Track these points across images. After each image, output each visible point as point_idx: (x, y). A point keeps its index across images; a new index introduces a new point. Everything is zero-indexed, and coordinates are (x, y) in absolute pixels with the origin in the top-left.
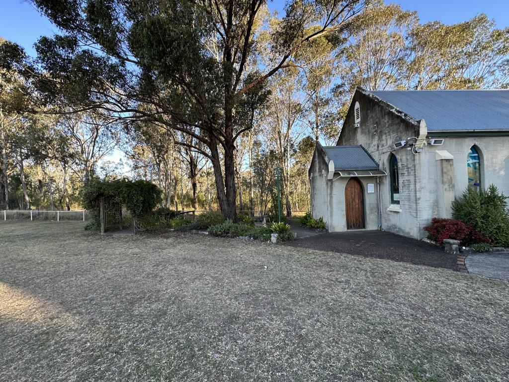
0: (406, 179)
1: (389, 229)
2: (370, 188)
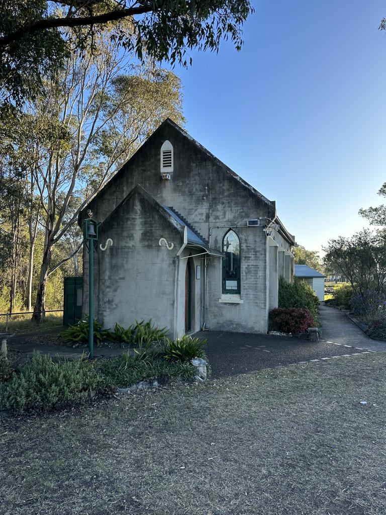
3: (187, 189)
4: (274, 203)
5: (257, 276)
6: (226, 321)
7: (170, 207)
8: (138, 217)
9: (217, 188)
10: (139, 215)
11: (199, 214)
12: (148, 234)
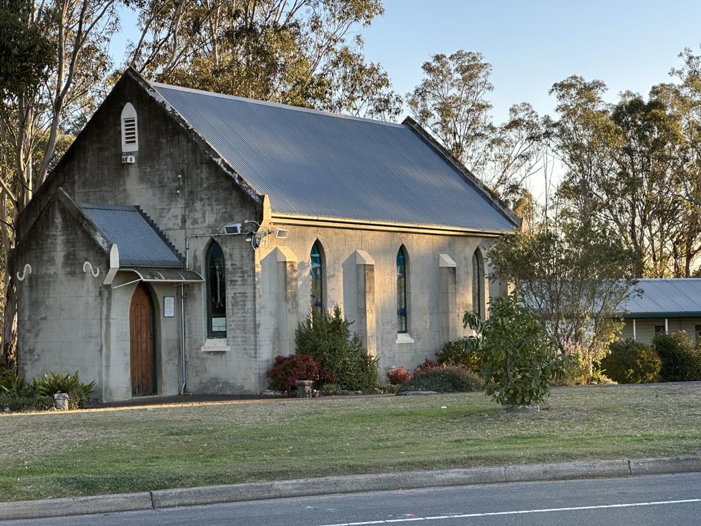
0: (239, 291)
1: (204, 388)
2: (169, 307)
3: (156, 179)
5: (245, 309)
6: (211, 378)
7: (135, 207)
8: (59, 233)
9: (194, 177)
10: (60, 231)
11: (173, 216)
12: (71, 257)
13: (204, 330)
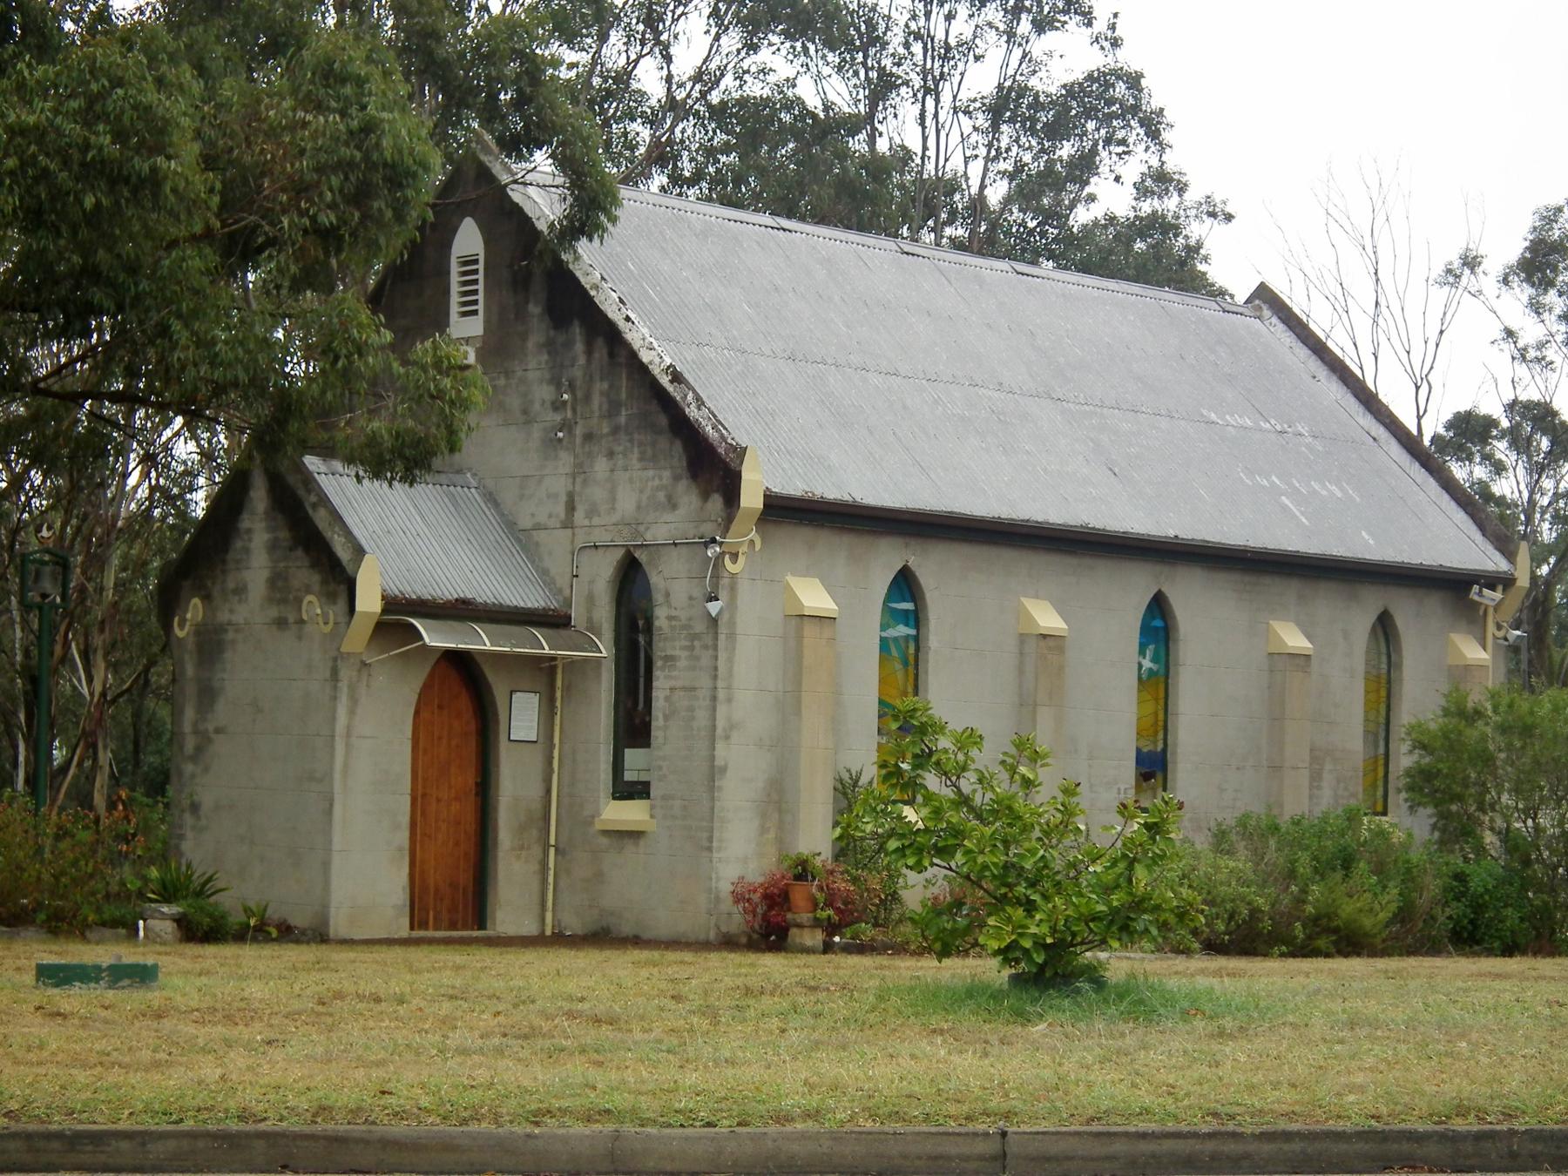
2: (522, 717)
4: (741, 452)
11: (549, 496)
13: (603, 776)
